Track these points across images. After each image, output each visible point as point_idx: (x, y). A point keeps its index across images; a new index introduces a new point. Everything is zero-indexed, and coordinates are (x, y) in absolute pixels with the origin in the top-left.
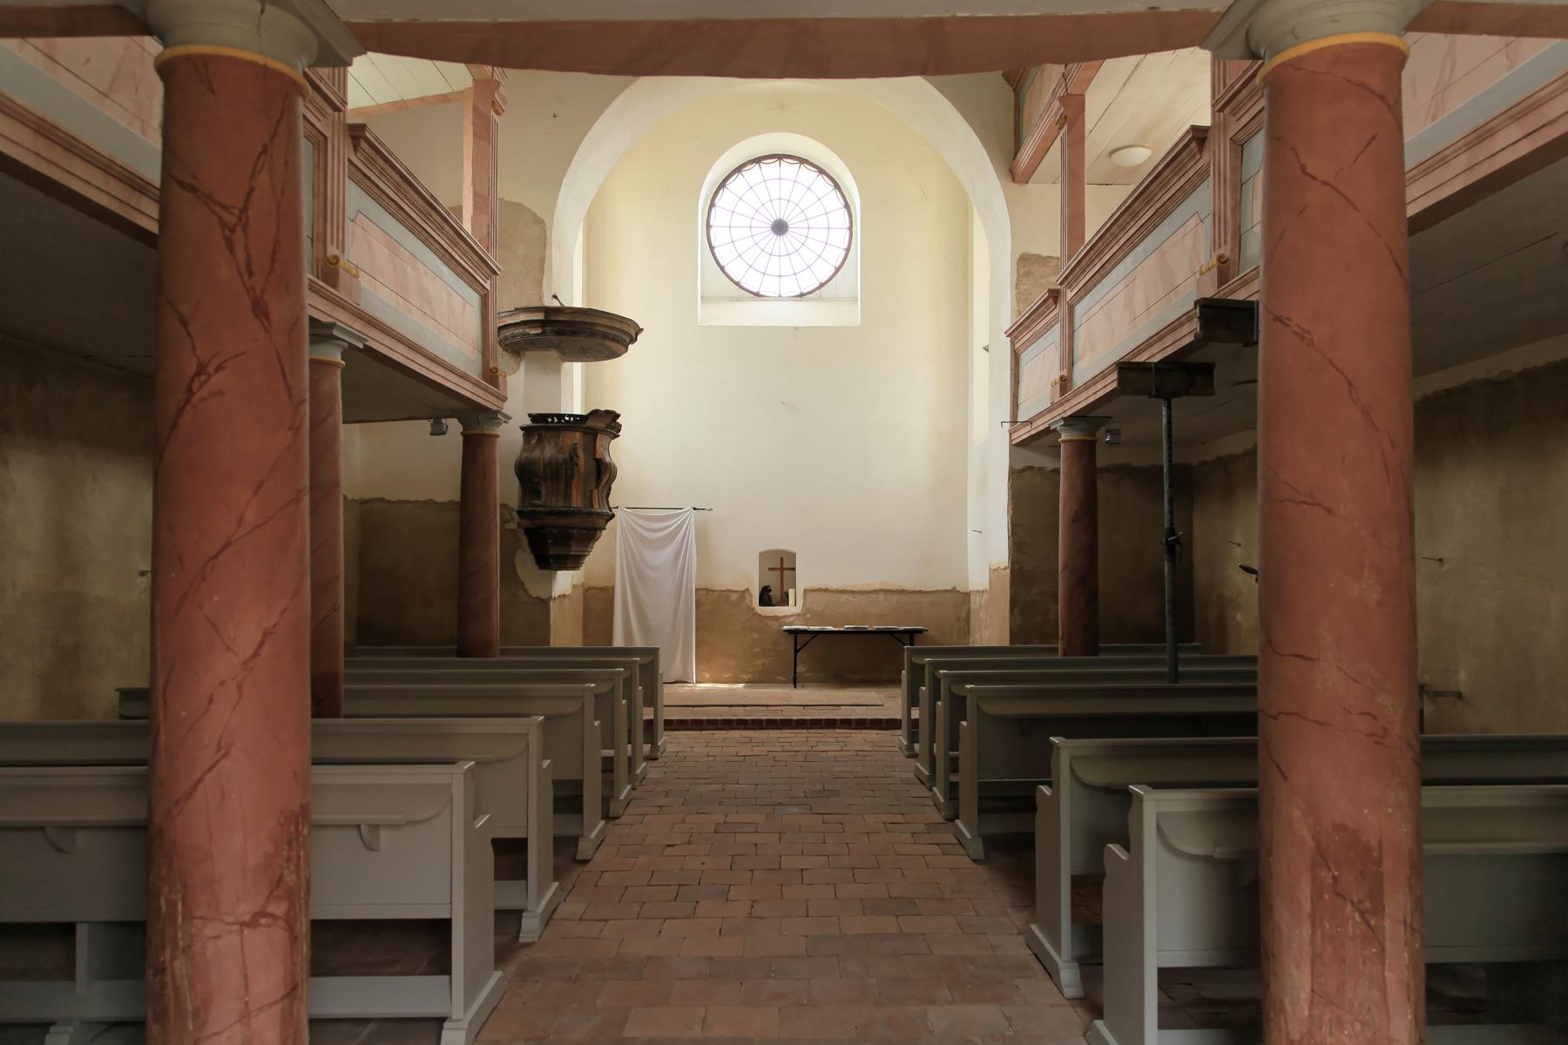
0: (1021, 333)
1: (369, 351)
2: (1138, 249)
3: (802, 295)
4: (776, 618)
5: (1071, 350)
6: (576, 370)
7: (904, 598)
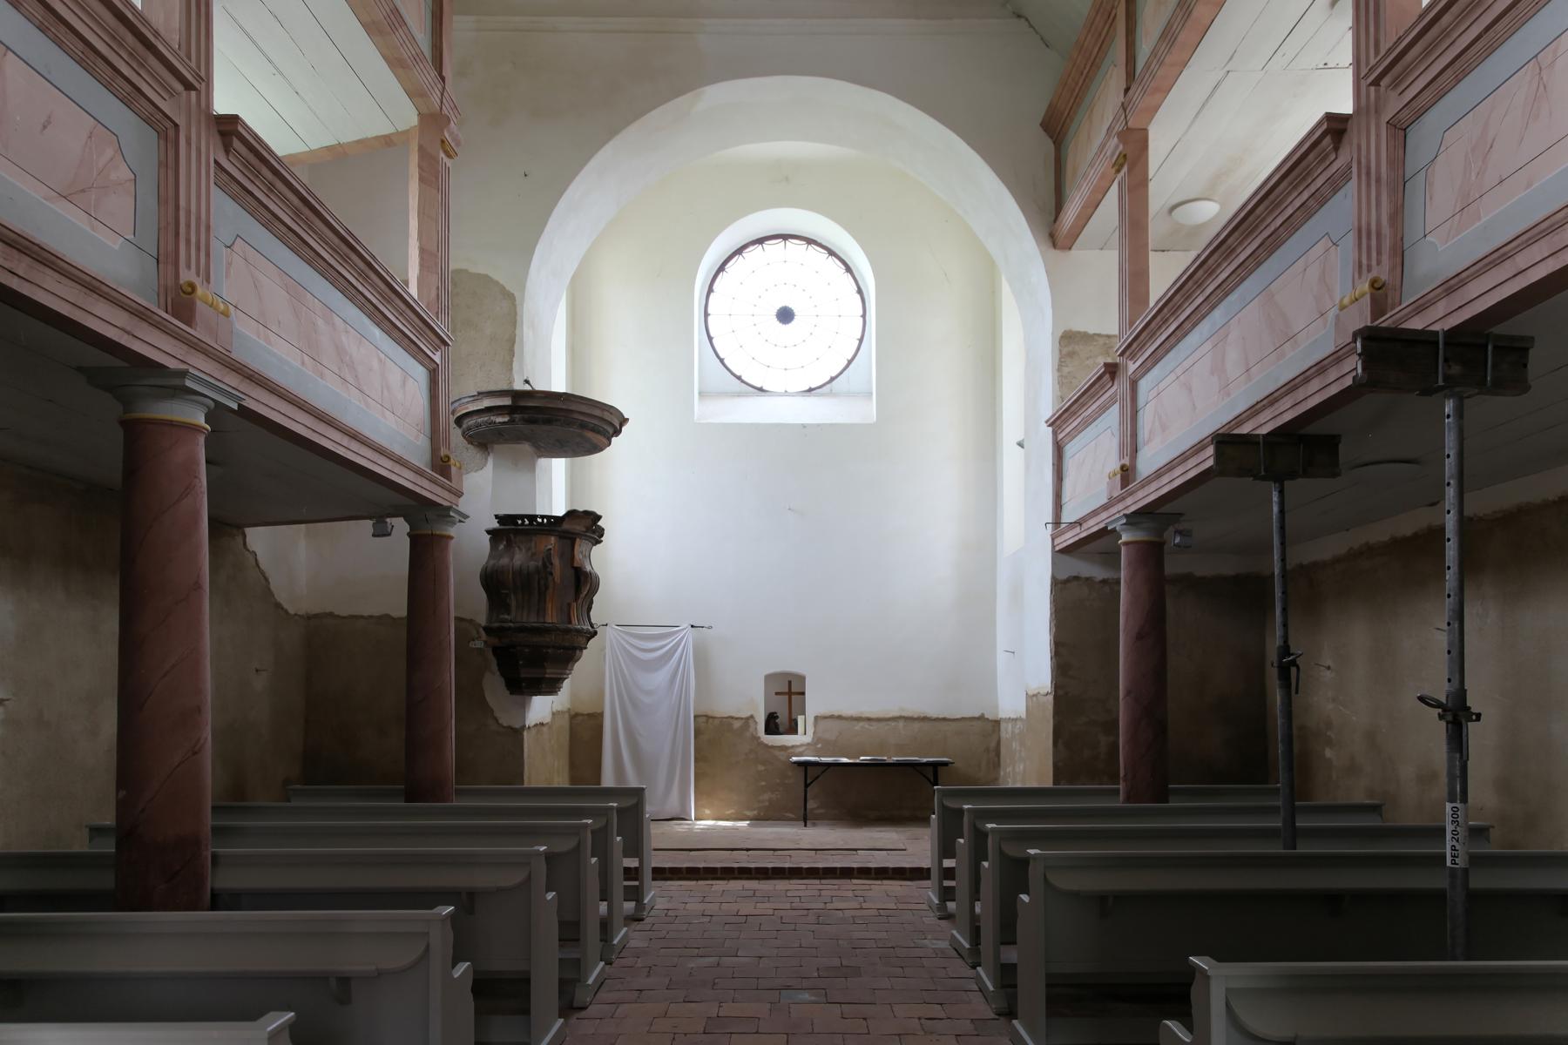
0: (1066, 421)
1: (244, 412)
2: (1233, 297)
3: (810, 390)
4: (784, 748)
5: (1134, 435)
6: (557, 468)
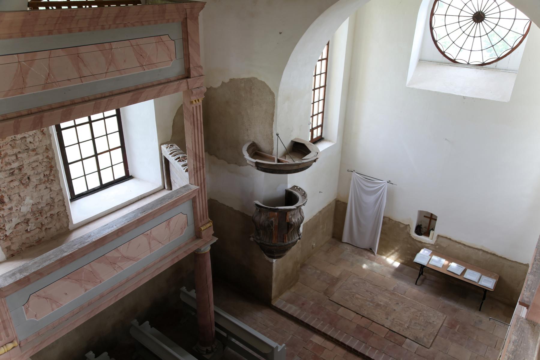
3: (483, 64)
7: (494, 258)
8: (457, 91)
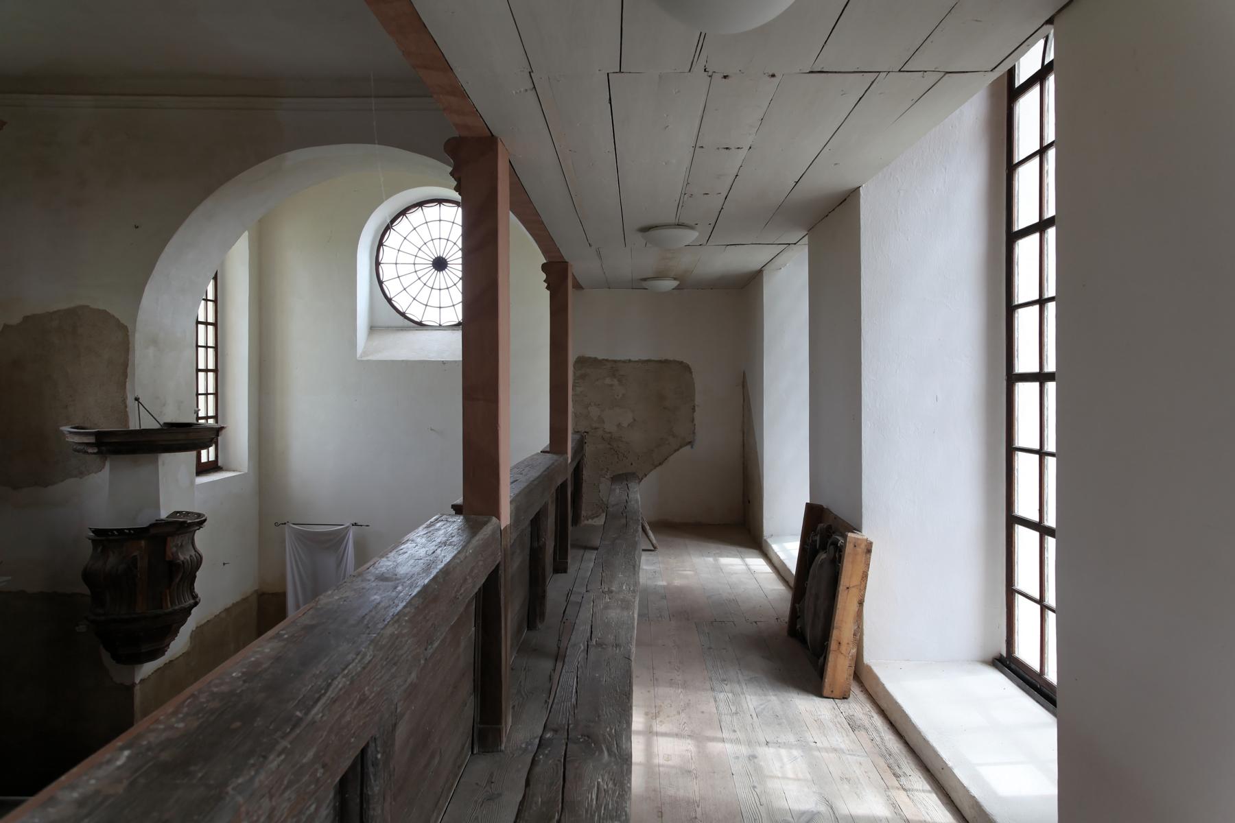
8: (433, 357)
